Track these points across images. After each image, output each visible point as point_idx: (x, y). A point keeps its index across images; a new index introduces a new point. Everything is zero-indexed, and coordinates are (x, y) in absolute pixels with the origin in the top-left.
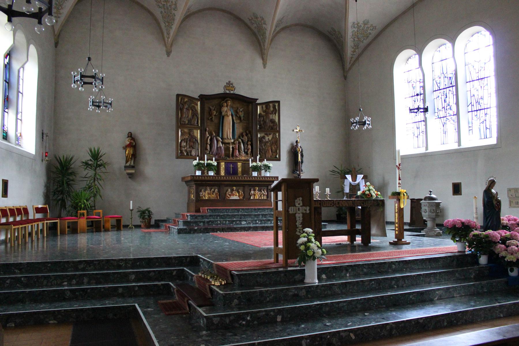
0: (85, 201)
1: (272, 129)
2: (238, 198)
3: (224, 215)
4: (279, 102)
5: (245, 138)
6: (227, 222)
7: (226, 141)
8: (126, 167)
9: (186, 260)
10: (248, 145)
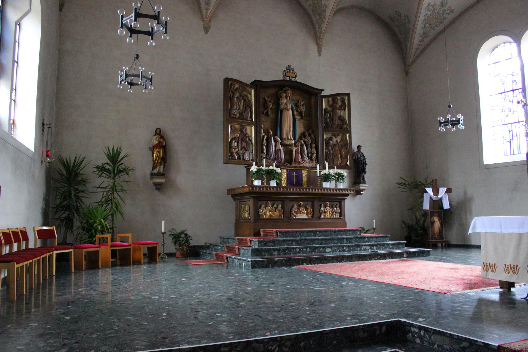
0: (102, 220)
1: (341, 128)
2: (306, 217)
3: (301, 240)
4: (348, 95)
5: (309, 140)
6: (308, 250)
7: (286, 142)
8: (153, 175)
9: (381, 330)
10: (311, 148)
